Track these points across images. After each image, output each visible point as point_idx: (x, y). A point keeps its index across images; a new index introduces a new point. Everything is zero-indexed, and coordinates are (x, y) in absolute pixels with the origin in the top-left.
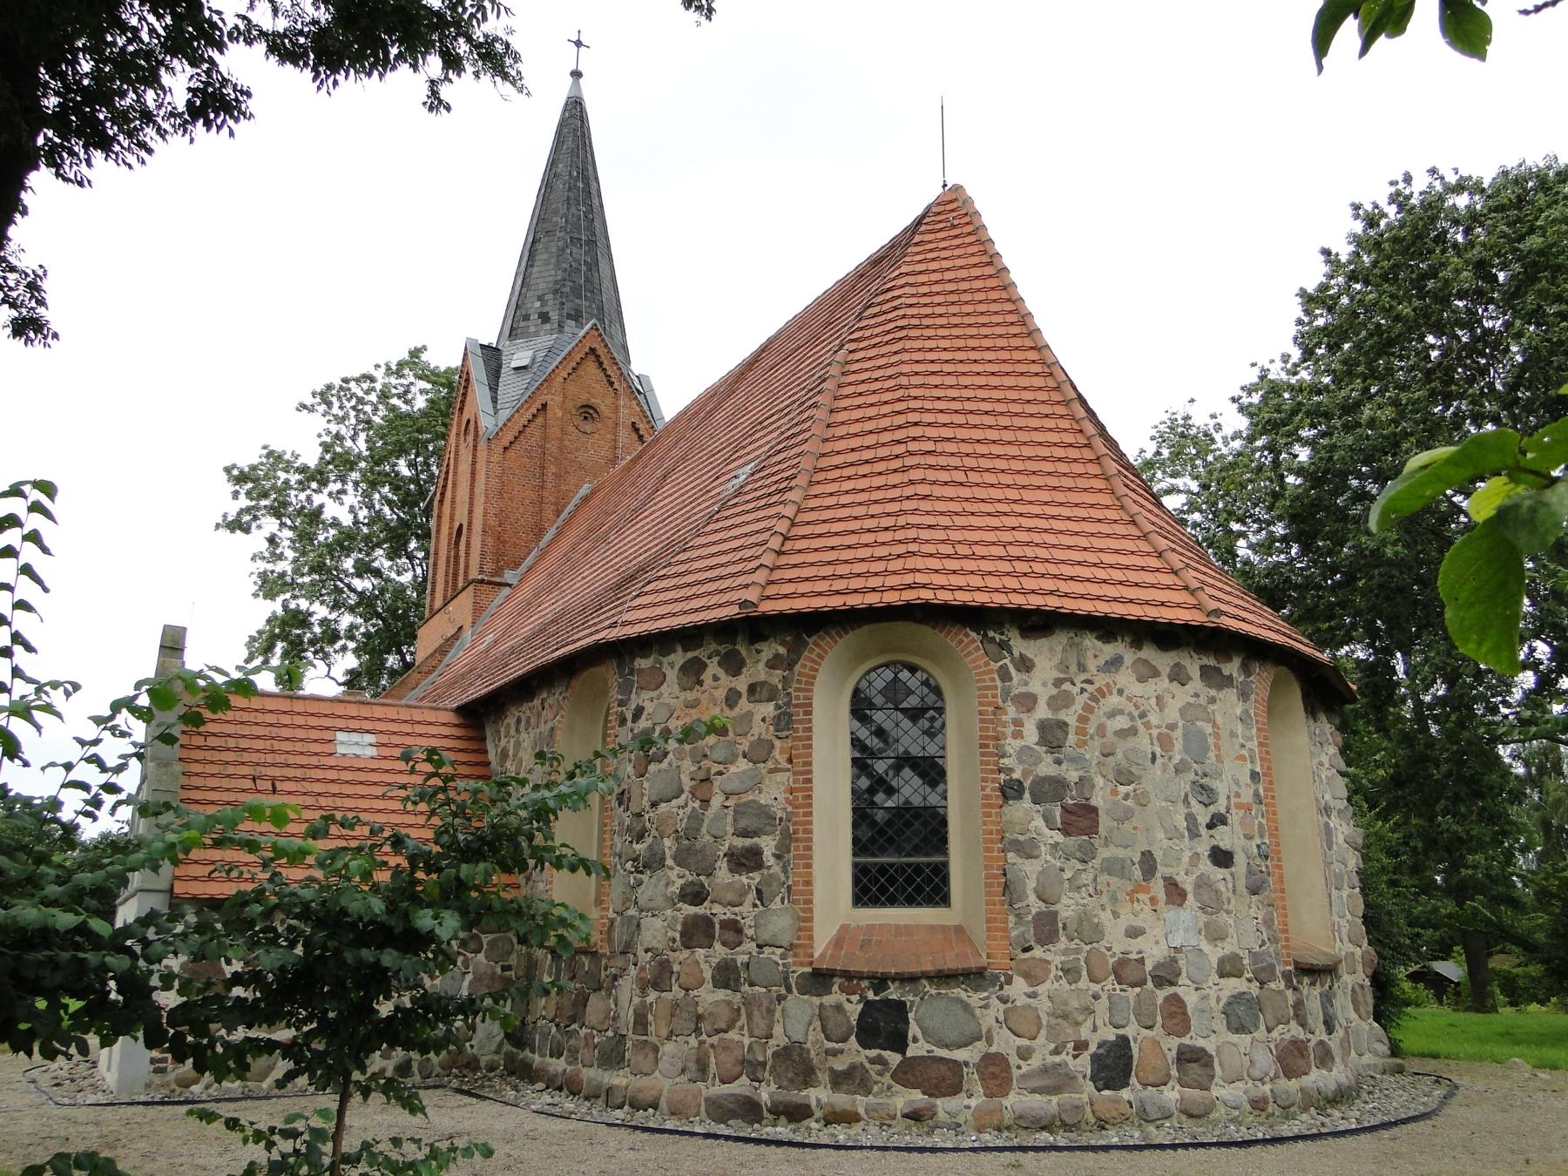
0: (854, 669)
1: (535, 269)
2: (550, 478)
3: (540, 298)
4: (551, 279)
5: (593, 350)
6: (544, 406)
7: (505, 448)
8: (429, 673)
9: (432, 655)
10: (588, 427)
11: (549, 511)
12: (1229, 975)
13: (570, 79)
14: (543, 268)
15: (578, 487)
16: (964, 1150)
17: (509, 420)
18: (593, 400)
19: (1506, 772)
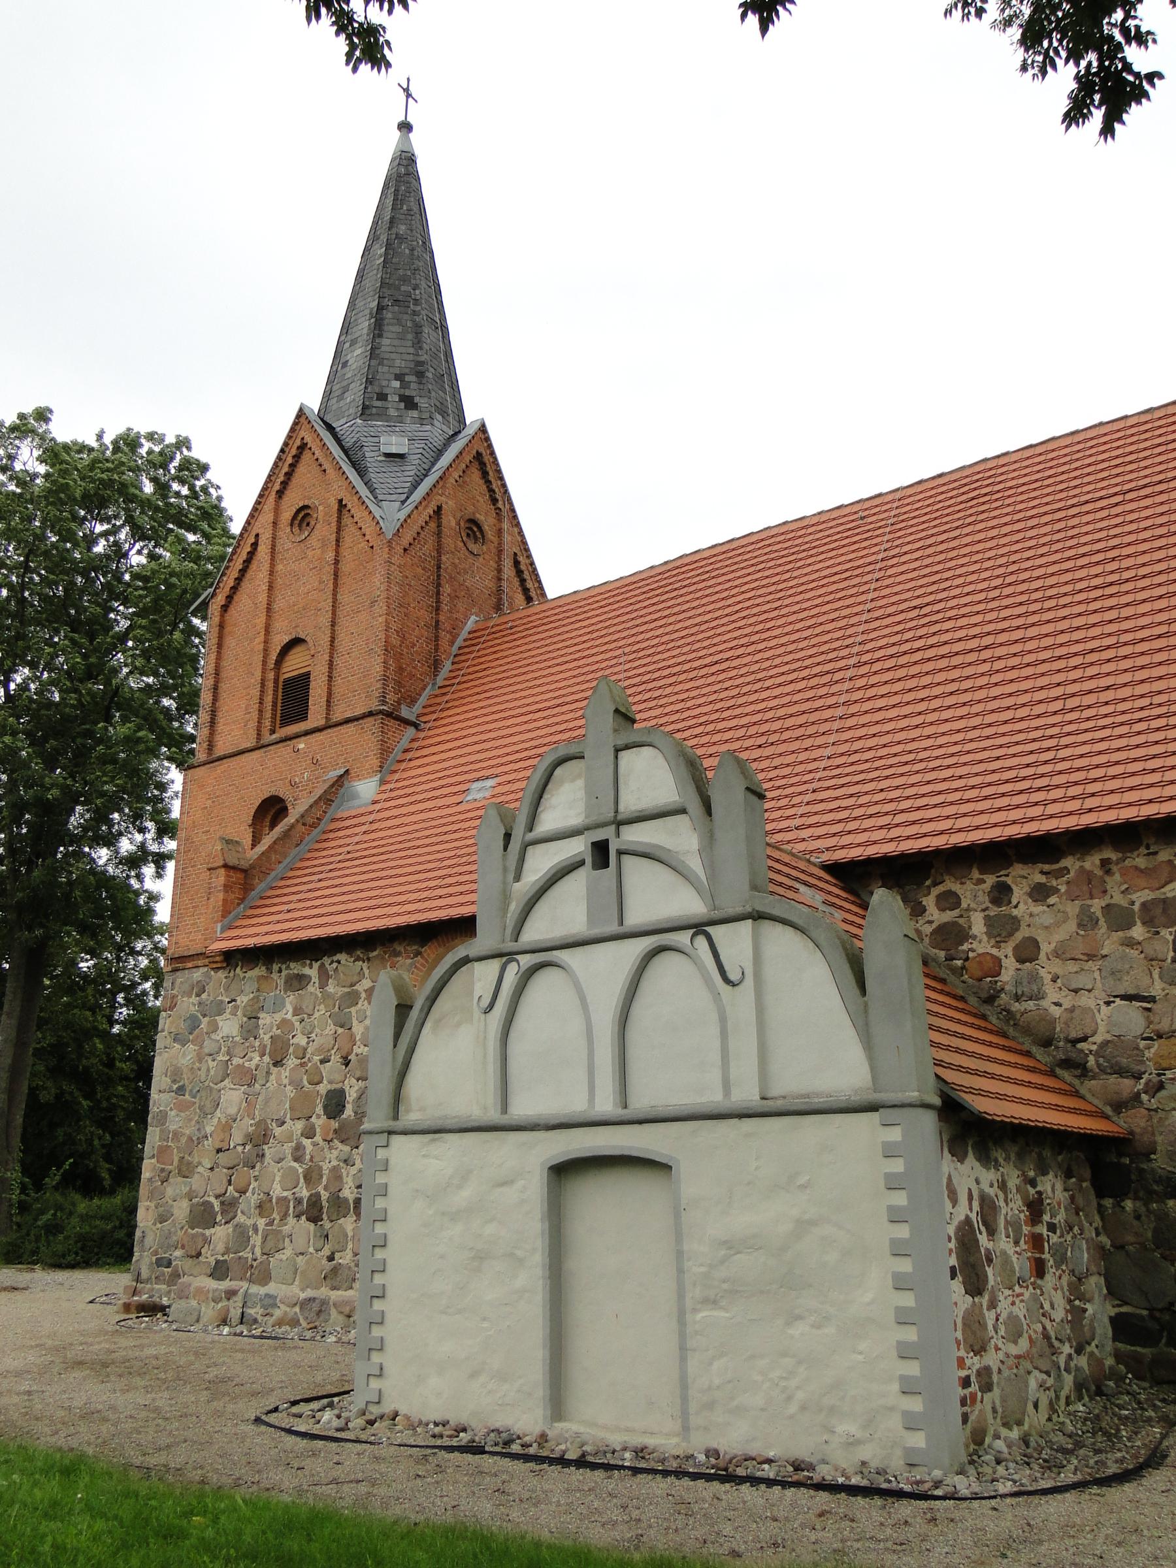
0: (265, 817)
1: (385, 342)
2: (445, 599)
3: (399, 377)
4: (411, 357)
5: (479, 455)
6: (439, 508)
7: (405, 550)
8: (314, 826)
9: (316, 802)
10: (474, 547)
11: (445, 637)
12: (304, 1054)
13: (397, 134)
14: (396, 342)
15: (467, 618)
16: (683, 1359)
17: (409, 516)
18: (478, 516)
19: (56, 853)
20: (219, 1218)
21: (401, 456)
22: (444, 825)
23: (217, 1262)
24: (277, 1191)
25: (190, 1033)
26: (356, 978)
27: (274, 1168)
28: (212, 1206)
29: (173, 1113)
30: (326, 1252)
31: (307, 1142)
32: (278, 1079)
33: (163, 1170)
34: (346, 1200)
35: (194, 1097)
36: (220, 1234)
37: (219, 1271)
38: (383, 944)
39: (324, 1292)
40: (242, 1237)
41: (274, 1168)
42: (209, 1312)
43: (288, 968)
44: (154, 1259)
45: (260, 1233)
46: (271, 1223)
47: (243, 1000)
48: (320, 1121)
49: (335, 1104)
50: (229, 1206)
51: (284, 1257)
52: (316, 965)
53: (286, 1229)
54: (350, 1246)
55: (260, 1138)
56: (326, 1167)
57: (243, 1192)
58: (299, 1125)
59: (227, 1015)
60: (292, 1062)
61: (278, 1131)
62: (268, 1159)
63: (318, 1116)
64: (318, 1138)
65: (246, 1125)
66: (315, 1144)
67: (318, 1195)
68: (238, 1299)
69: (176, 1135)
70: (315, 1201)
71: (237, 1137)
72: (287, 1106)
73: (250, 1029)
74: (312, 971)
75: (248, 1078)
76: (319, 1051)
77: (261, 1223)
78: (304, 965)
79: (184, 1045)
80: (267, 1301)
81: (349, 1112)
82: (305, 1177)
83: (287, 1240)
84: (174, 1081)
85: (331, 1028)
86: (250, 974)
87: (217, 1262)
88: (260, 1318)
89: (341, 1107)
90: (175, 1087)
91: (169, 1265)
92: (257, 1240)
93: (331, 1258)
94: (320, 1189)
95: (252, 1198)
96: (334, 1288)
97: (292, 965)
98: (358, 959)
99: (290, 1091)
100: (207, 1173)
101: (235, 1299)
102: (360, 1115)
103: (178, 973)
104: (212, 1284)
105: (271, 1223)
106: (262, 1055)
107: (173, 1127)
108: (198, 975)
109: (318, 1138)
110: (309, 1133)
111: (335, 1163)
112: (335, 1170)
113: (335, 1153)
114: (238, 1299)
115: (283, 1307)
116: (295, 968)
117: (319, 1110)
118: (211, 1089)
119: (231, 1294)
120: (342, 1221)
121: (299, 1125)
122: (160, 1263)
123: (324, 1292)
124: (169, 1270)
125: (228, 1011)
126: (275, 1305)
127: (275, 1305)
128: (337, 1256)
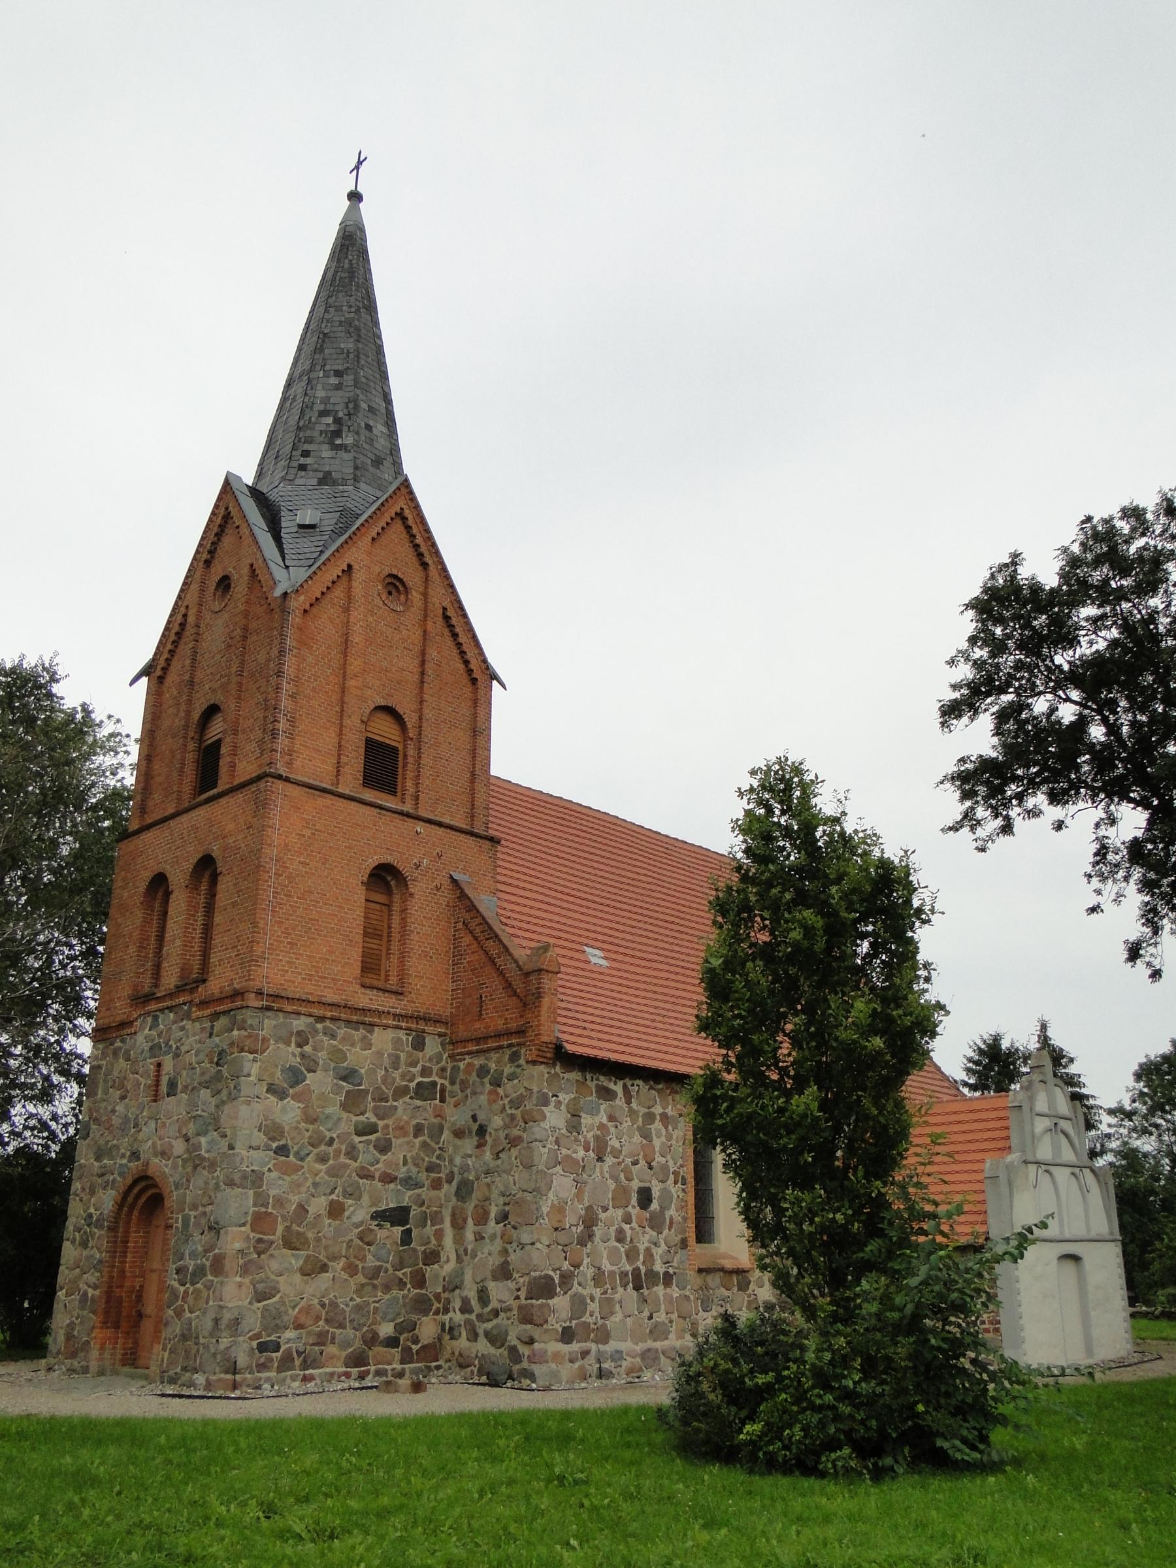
20: (558, 1289)
21: (312, 527)
22: (575, 975)
23: (564, 1328)
24: (607, 1266)
25: (291, 1087)
26: (651, 1103)
27: (602, 1246)
28: (553, 1280)
29: (274, 1174)
30: (646, 1314)
31: (626, 1227)
32: (602, 1173)
33: (260, 1241)
34: (658, 1273)
35: (302, 1160)
36: (561, 1303)
37: (567, 1336)
38: (666, 1082)
39: (650, 1344)
40: (579, 1306)
41: (602, 1246)
42: (567, 1370)
43: (598, 1079)
44: (255, 1344)
45: (597, 1300)
46: (605, 1292)
47: (564, 1097)
48: (634, 1211)
49: (645, 1197)
50: (566, 1278)
51: (617, 1320)
52: (620, 1083)
53: (617, 1297)
54: (663, 1307)
55: (589, 1221)
56: (642, 1248)
57: (577, 1266)
58: (620, 1213)
59: (551, 1107)
60: (609, 1160)
61: (602, 1216)
62: (597, 1238)
63: (634, 1207)
64: (634, 1224)
65: (580, 1208)
66: (632, 1229)
67: (638, 1269)
68: (591, 1359)
69: (280, 1202)
70: (636, 1273)
71: (570, 1220)
72: (610, 1196)
73: (574, 1126)
74: (618, 1088)
75: (576, 1169)
76: (631, 1155)
77: (597, 1292)
78: (610, 1080)
79: (281, 1099)
80: (617, 1356)
81: (655, 1206)
82: (627, 1256)
83: (618, 1306)
84: (273, 1139)
85: (637, 1138)
86: (567, 1076)
87: (564, 1328)
88: (614, 1371)
89: (650, 1200)
90: (274, 1145)
91: (277, 1348)
92: (594, 1307)
93: (650, 1318)
94: (639, 1264)
95: (587, 1271)
96: (655, 1340)
97: (602, 1078)
98: (651, 1088)
99: (612, 1185)
100: (545, 1250)
101: (588, 1357)
102: (663, 1209)
103: (269, 1013)
104: (565, 1348)
105: (605, 1292)
106: (587, 1149)
107: (273, 1192)
108: (299, 1023)
109: (634, 1224)
110: (627, 1220)
111: (646, 1244)
112: (648, 1250)
113: (647, 1237)
114: (591, 1359)
115: (628, 1359)
116: (604, 1081)
117: (634, 1201)
118: (545, 1173)
119: (585, 1353)
120: (655, 1289)
121: (620, 1213)
122: (263, 1347)
123: (650, 1344)
124: (279, 1354)
125: (553, 1104)
126: (622, 1358)
127: (622, 1358)
128: (654, 1315)
